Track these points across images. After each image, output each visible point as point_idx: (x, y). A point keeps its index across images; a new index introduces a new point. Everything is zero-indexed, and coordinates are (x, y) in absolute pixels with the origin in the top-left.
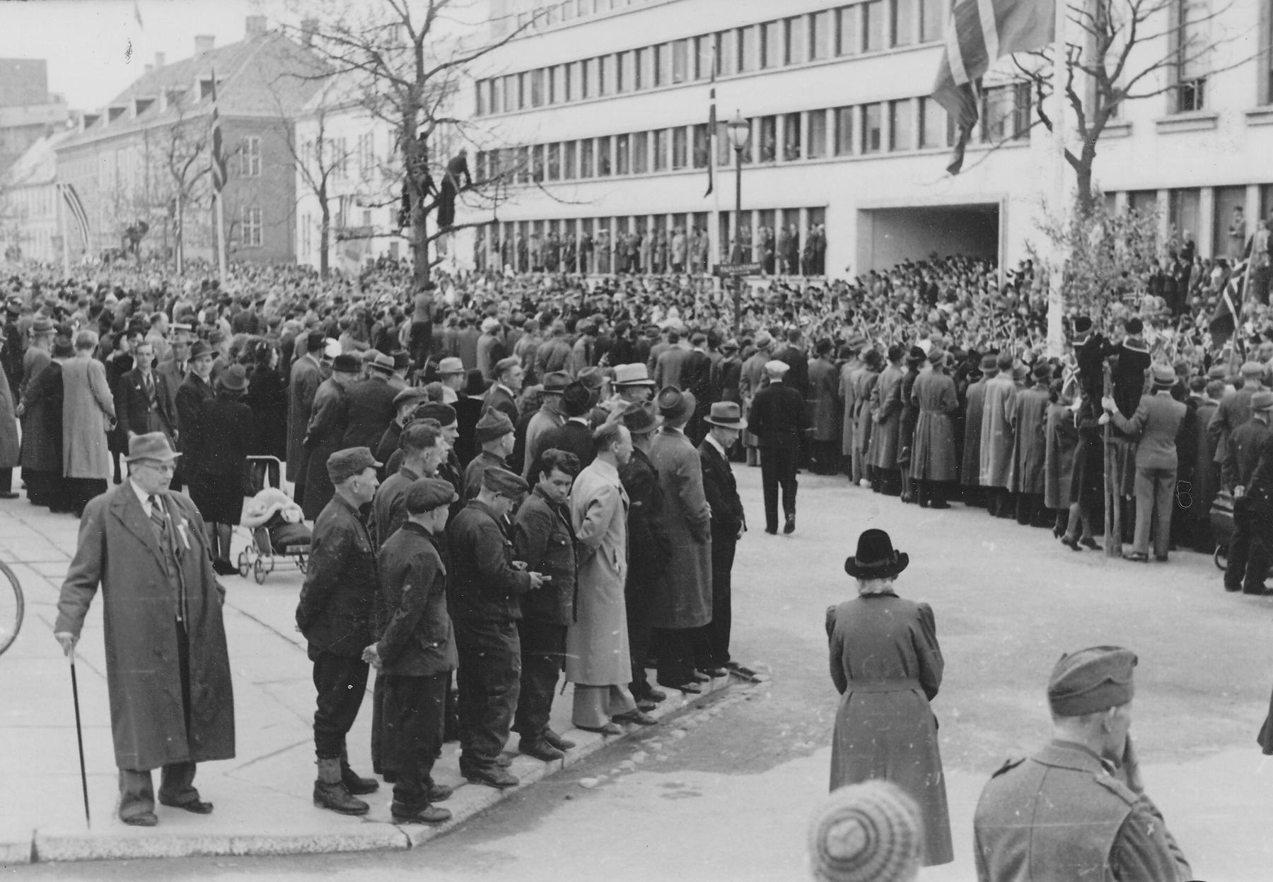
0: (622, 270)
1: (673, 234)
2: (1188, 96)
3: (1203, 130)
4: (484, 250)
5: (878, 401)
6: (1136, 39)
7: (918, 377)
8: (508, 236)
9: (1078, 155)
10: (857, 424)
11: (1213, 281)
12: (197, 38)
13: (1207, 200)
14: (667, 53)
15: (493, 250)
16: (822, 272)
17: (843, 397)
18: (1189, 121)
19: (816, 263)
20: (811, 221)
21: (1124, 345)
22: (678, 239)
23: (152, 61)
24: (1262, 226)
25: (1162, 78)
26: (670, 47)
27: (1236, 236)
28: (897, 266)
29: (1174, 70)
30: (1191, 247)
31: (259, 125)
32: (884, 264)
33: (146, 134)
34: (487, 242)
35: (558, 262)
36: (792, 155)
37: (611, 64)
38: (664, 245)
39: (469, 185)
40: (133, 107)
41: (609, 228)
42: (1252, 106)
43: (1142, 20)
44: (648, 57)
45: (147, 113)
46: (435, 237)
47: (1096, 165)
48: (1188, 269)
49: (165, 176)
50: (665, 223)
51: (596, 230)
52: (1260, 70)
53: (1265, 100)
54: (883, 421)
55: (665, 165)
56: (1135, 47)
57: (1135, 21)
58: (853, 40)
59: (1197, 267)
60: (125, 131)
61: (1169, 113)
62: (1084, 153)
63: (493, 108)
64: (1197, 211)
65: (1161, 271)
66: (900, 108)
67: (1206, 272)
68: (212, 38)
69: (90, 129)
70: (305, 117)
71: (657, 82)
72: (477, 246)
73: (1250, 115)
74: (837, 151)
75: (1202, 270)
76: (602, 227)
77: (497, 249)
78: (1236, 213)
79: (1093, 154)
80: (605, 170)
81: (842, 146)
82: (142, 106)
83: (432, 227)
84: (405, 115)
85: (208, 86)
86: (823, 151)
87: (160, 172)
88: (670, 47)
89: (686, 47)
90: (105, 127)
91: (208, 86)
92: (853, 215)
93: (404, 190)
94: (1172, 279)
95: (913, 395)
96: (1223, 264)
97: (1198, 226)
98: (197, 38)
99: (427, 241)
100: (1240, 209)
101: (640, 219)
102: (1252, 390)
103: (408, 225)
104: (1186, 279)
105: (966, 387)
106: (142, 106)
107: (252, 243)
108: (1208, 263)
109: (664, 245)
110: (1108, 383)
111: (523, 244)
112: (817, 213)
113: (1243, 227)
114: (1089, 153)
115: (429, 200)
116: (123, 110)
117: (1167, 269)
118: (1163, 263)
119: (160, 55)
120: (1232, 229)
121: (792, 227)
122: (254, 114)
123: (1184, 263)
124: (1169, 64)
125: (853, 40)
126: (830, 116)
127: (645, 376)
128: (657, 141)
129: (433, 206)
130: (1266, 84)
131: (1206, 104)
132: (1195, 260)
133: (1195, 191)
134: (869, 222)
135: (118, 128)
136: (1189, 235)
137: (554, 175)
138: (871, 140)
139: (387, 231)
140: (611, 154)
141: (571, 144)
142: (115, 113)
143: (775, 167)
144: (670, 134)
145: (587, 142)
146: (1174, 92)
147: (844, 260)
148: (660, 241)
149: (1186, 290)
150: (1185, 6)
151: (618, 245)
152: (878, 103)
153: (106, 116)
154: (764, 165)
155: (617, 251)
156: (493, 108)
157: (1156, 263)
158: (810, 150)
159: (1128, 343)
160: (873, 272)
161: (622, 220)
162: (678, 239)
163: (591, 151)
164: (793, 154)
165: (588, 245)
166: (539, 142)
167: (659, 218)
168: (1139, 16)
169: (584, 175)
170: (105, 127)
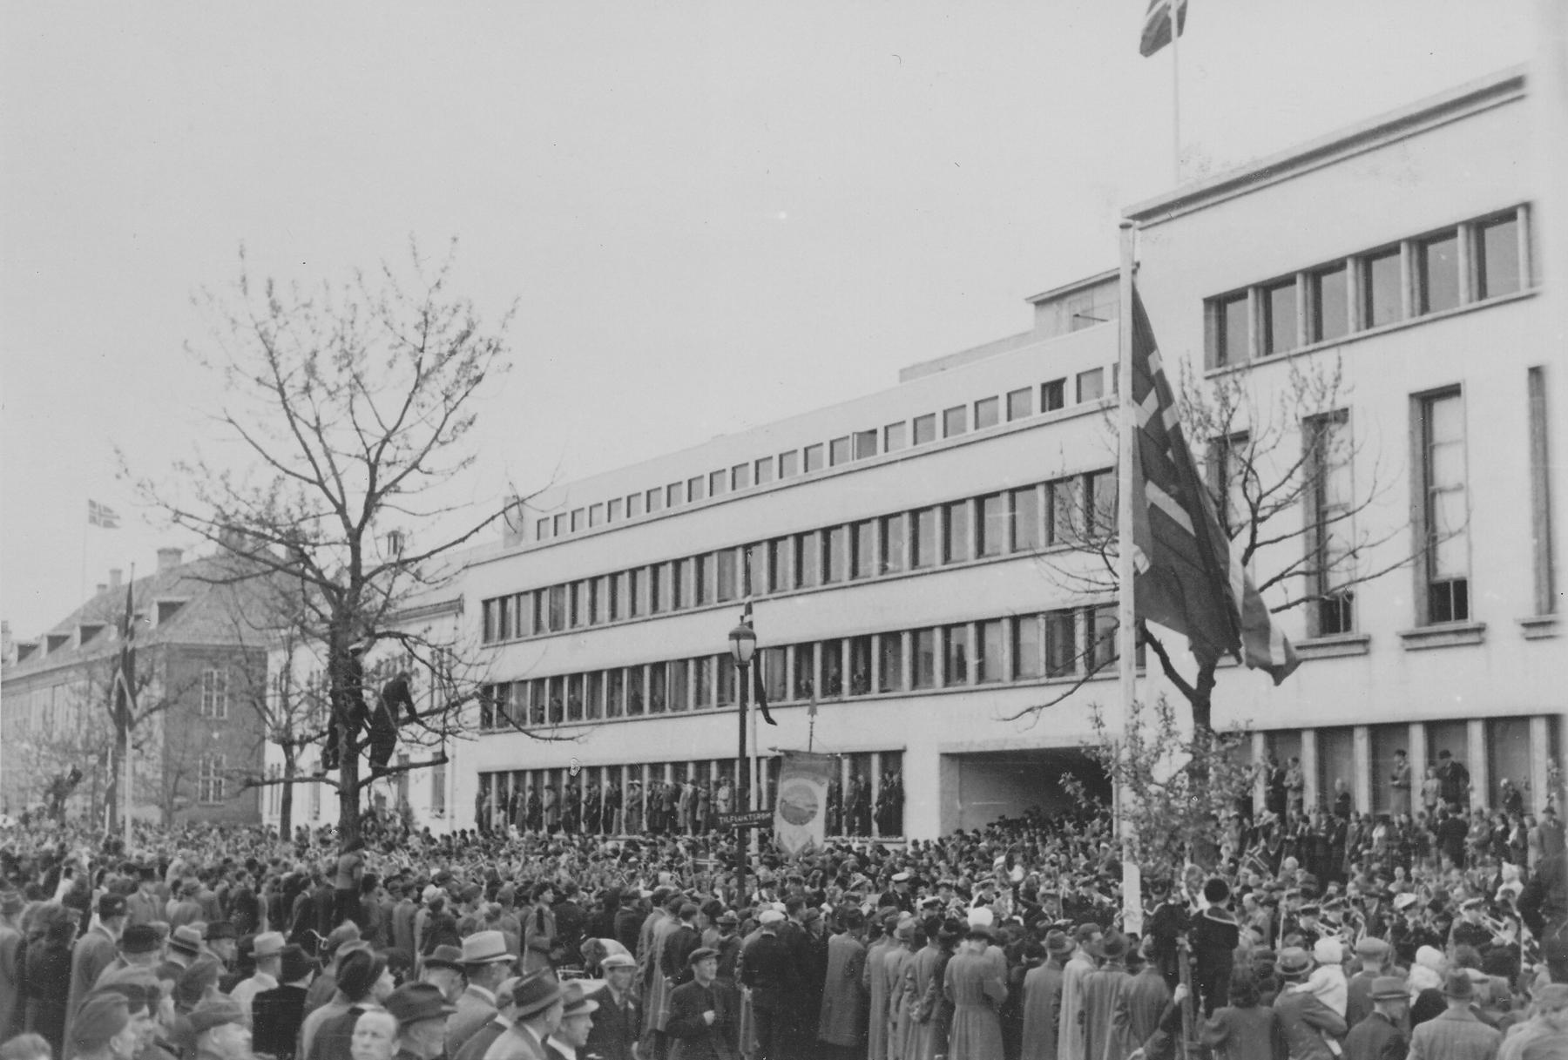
0: (655, 830)
1: (718, 785)
2: (1333, 614)
3: (1353, 655)
4: (489, 807)
5: (916, 991)
6: (1258, 541)
7: (952, 960)
8: (517, 788)
9: (1193, 682)
10: (895, 1025)
11: (1375, 842)
12: (160, 552)
13: (1361, 744)
14: (711, 566)
15: (499, 809)
16: (899, 832)
17: (869, 987)
18: (1335, 644)
19: (892, 822)
20: (884, 768)
21: (1205, 915)
22: (724, 793)
23: (106, 579)
24: (1430, 773)
25: (1297, 587)
26: (715, 557)
27: (1399, 787)
28: (992, 825)
29: (1314, 578)
30: (1347, 799)
31: (215, 656)
32: (973, 823)
33: (89, 666)
34: (493, 797)
35: (578, 822)
36: (860, 688)
37: (645, 579)
38: (707, 799)
39: (414, 717)
40: (77, 635)
41: (641, 778)
42: (1409, 626)
43: (1264, 519)
44: (689, 571)
45: (94, 642)
46: (368, 781)
47: (1216, 696)
48: (1344, 827)
49: (101, 715)
50: (686, 772)
51: (625, 780)
52: (1416, 583)
53: (1425, 618)
54: (924, 1020)
55: (709, 702)
56: (1257, 551)
57: (1256, 520)
58: (932, 550)
59: (1354, 825)
60: (65, 664)
61: (1311, 636)
62: (1200, 680)
63: (504, 633)
64: (1350, 755)
65: (1311, 830)
66: (990, 630)
67: (1366, 830)
68: (178, 552)
69: (24, 662)
70: (275, 647)
71: (700, 600)
72: (480, 800)
73: (1407, 637)
74: (915, 683)
75: (1361, 829)
76: (632, 777)
77: (504, 807)
78: (1397, 758)
79: (1213, 683)
80: (636, 707)
81: (922, 673)
82: (88, 633)
83: (364, 770)
84: (331, 627)
85: (168, 610)
86: (898, 682)
87: (94, 714)
88: (715, 557)
89: (734, 558)
90: (43, 659)
91: (168, 610)
92: (936, 759)
93: (333, 721)
94: (1326, 839)
95: (946, 983)
96: (1386, 820)
97: (1353, 775)
98: (160, 552)
99: (357, 786)
100: (1403, 753)
101: (679, 767)
102: (1371, 974)
103: (335, 767)
104: (1341, 841)
105: (1023, 973)
106: (88, 633)
107: (211, 800)
108: (1367, 818)
109: (707, 799)
110: (1185, 966)
111: (535, 799)
112: (892, 759)
113: (1408, 774)
114: (1207, 680)
115: (363, 735)
116: (65, 638)
117: (1319, 825)
118: (1313, 818)
119: (116, 573)
120: (1395, 779)
121: (861, 777)
122: (208, 641)
123: (1339, 821)
124: (1307, 574)
125: (932, 550)
126: (906, 640)
127: (503, 948)
128: (699, 673)
129: (366, 742)
130: (1425, 600)
131: (1354, 625)
132: (1352, 816)
133: (1347, 731)
134: (954, 772)
135: (62, 657)
136: (1343, 785)
137: (575, 713)
138: (955, 669)
139: (308, 774)
140: (647, 688)
141: (596, 675)
142: (56, 642)
143: (840, 702)
144: (715, 662)
145: (616, 673)
146: (1314, 606)
147: (924, 820)
148: (702, 795)
149: (1343, 854)
150: (1323, 507)
151: (650, 800)
152: (964, 624)
153: (45, 644)
154: (827, 699)
155: (650, 807)
156: (504, 633)
157: (1306, 820)
158: (882, 683)
159: (1210, 912)
160: (960, 832)
161: (656, 768)
162: (724, 793)
163: (620, 684)
164: (862, 685)
165: (615, 799)
166: (556, 673)
167: (702, 765)
168: (1260, 514)
169: (611, 713)
170: (43, 659)
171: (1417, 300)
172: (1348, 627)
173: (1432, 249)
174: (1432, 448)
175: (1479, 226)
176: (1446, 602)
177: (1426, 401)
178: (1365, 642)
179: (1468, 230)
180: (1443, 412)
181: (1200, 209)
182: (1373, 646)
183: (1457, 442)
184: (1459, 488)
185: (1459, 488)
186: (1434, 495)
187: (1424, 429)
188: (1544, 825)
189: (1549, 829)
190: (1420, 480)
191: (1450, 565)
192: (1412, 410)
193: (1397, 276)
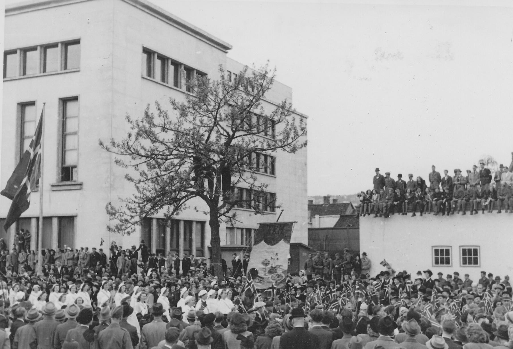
171: (63, 65)
172: (72, 179)
173: (70, 48)
174: (24, 123)
175: (66, 44)
176: (67, 173)
177: (64, 101)
178: (81, 184)
179: (41, 48)
180: (71, 106)
181: (36, 10)
182: (84, 187)
183: (75, 117)
184: (75, 133)
185: (75, 133)
186: (65, 135)
187: (63, 113)
188: (13, 254)
189: (14, 255)
190: (61, 129)
191: (70, 161)
192: (18, 108)
193: (54, 56)
